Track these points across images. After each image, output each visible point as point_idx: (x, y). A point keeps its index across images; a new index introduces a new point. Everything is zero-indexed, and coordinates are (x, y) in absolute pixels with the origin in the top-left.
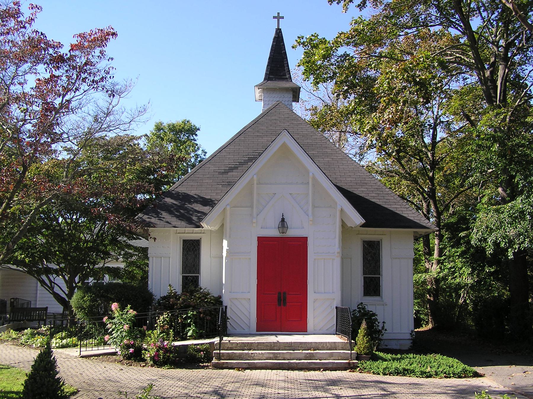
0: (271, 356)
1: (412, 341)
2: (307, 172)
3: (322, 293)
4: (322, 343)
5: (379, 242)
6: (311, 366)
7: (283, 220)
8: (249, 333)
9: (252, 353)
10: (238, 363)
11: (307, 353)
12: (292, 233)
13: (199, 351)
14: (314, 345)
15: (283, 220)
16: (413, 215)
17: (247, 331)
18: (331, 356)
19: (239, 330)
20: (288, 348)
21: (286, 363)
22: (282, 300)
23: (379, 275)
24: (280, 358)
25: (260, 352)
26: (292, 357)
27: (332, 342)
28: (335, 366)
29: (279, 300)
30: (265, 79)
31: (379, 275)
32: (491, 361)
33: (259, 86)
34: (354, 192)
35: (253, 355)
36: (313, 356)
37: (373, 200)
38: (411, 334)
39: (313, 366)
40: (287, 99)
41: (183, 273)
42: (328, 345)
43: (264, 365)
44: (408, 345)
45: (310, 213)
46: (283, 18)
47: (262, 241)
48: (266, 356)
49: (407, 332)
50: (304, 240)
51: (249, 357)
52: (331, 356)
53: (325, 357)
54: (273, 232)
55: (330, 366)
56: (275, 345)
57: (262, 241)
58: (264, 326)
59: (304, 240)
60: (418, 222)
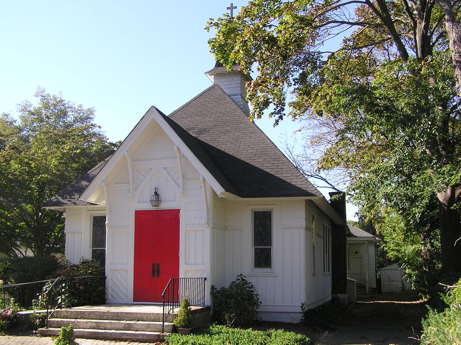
0: (94, 325)
1: (303, 315)
2: (174, 144)
3: (193, 264)
4: (146, 313)
5: (255, 212)
6: (124, 337)
7: (156, 194)
8: (126, 303)
9: (78, 322)
10: (106, 332)
11: (126, 324)
12: (165, 206)
13: (37, 318)
14: (139, 316)
15: (156, 194)
16: (301, 183)
17: (125, 301)
18: (148, 327)
19: (119, 300)
20: (115, 318)
21: (103, 333)
22: (156, 271)
23: (271, 246)
24: (102, 328)
25: (85, 320)
26: (113, 327)
27: (155, 314)
28: (145, 338)
29: (153, 271)
30: (216, 66)
31: (271, 246)
32: (365, 338)
33: (210, 73)
34: (251, 163)
35: (78, 324)
36: (132, 327)
37: (266, 170)
38: (302, 307)
39: (125, 337)
40: (235, 83)
41: (93, 247)
42: (152, 316)
43: (81, 334)
44: (298, 318)
45: (181, 186)
46: (232, 4)
47: (140, 215)
48: (90, 325)
49: (298, 305)
50: (177, 212)
51: (75, 325)
52: (148, 327)
53: (142, 328)
54: (148, 206)
55: (141, 337)
56: (104, 314)
57: (140, 215)
58: (140, 297)
59: (177, 212)
60: (305, 189)
